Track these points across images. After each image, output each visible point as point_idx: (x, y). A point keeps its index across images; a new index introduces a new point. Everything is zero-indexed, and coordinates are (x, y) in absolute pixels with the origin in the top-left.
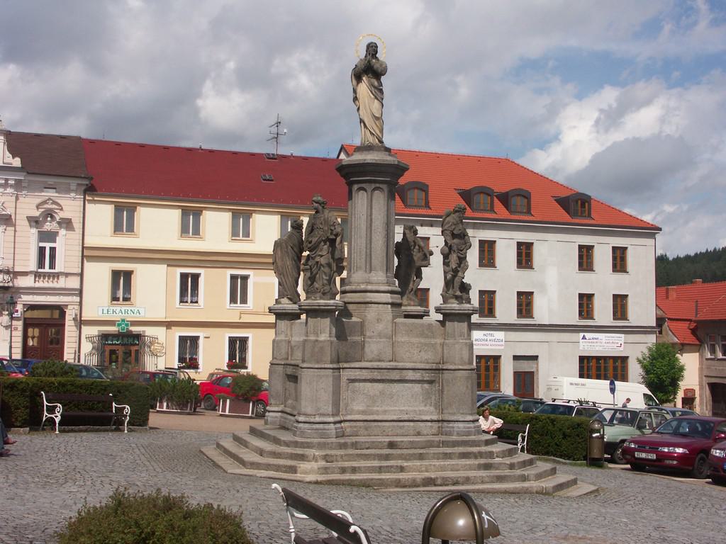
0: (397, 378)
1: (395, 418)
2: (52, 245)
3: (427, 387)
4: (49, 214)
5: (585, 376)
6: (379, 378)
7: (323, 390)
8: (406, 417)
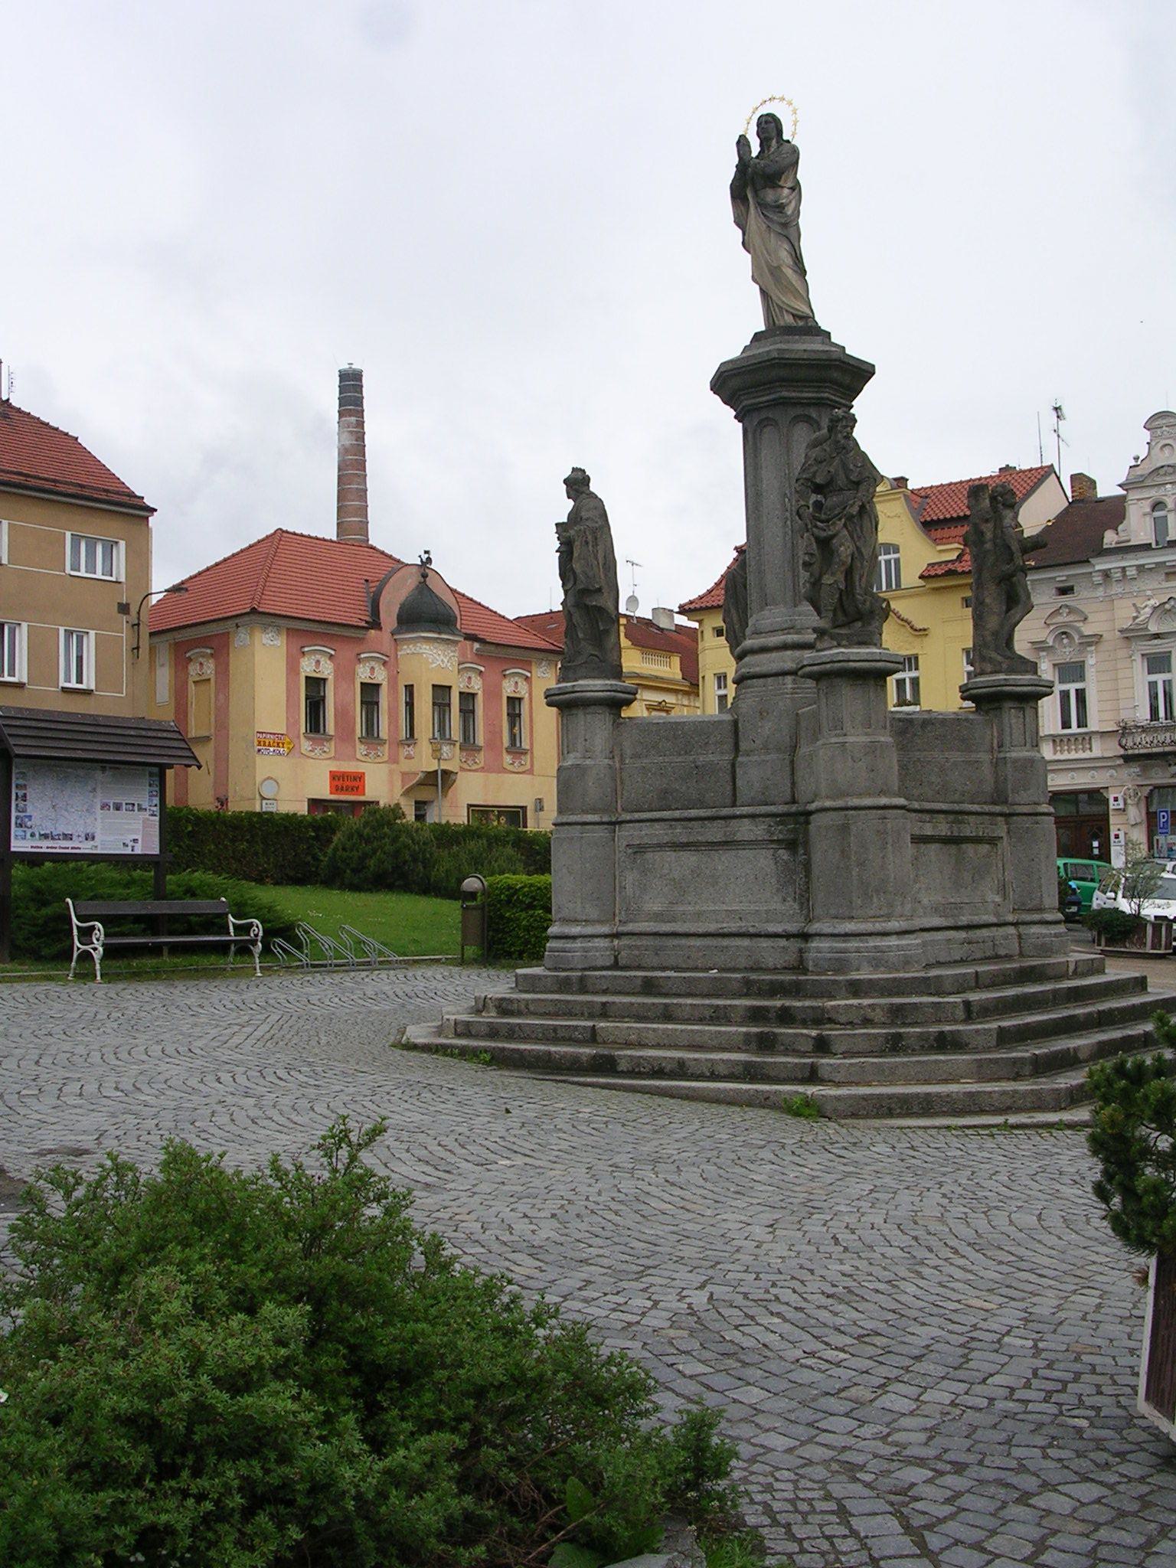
0: (719, 837)
1: (712, 927)
2: (1079, 686)
3: (785, 857)
4: (1064, 633)
5: (336, 783)
6: (685, 840)
7: (564, 870)
8: (733, 926)
